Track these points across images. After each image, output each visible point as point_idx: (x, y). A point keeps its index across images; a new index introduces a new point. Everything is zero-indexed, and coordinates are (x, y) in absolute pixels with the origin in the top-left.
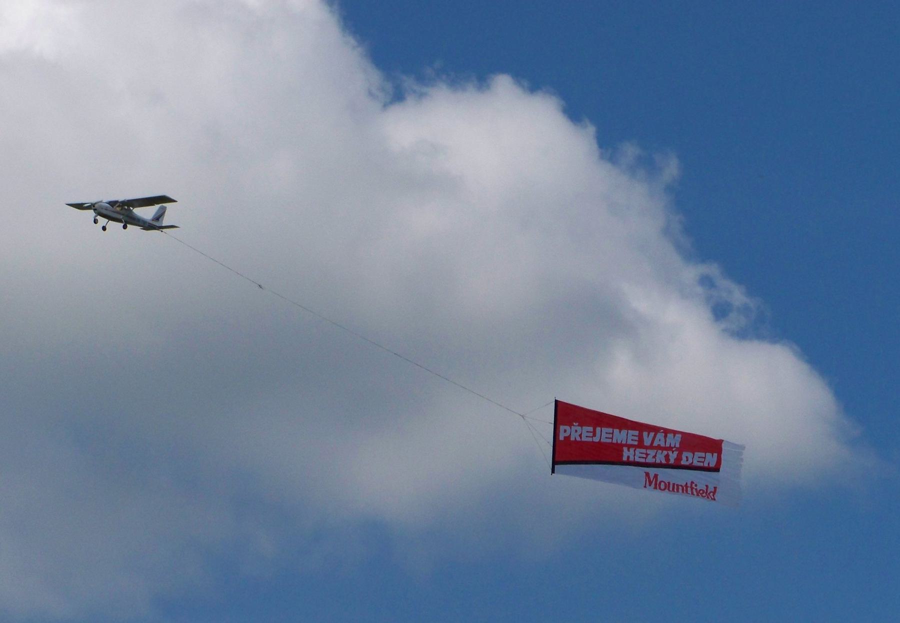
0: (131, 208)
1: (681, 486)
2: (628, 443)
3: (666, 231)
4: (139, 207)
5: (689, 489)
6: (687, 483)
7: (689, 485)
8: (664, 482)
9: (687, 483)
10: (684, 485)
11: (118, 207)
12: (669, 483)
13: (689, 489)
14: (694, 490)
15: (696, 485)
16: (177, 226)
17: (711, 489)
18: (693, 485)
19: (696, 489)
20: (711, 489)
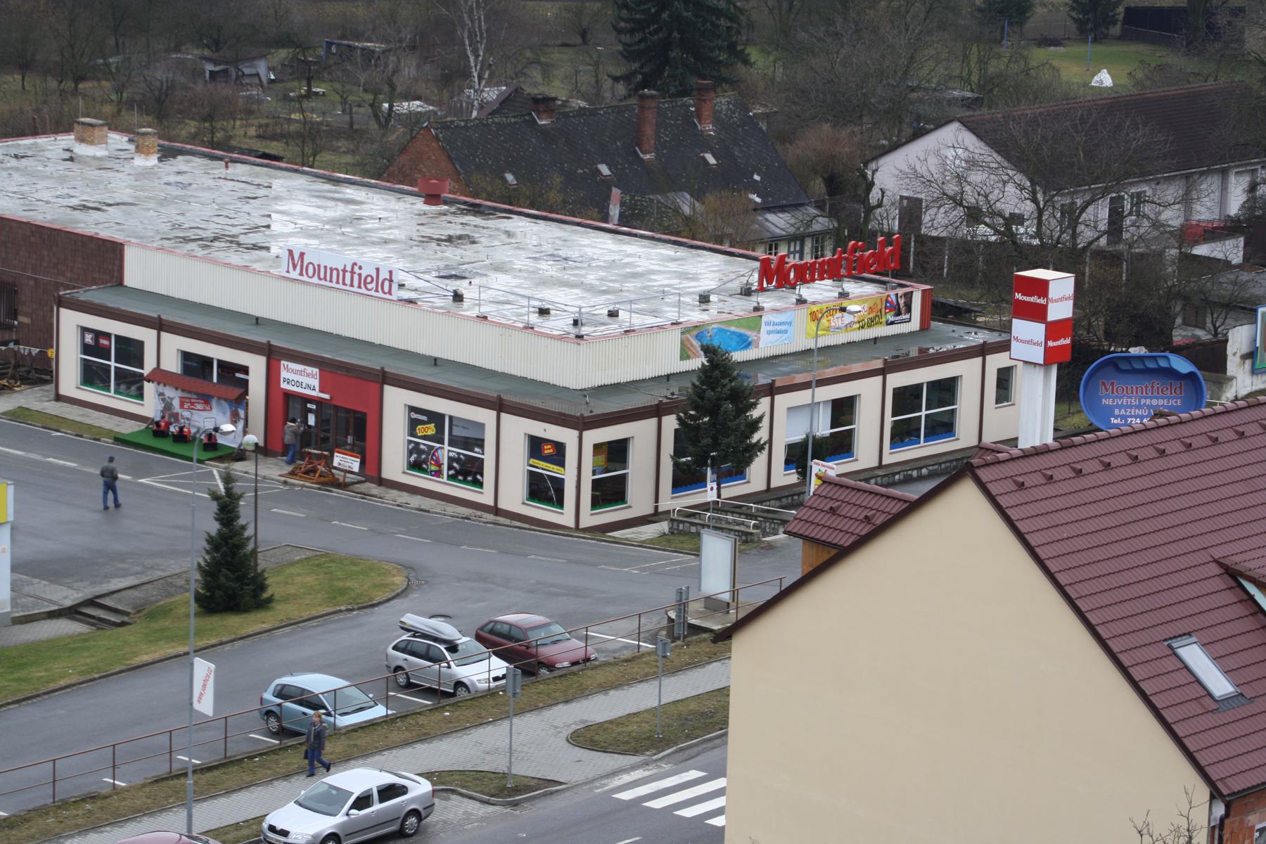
0: (208, 594)
1: (337, 269)
2: (885, 462)
3: (441, 740)
4: (998, 378)
5: (348, 275)
6: (345, 266)
7: (349, 268)
8: (313, 265)
9: (345, 266)
10: (340, 268)
11: (351, 808)
12: (319, 266)
13: (348, 275)
14: (356, 278)
15: (360, 268)
16: (561, 780)
17: (384, 275)
18: (356, 269)
19: (360, 275)
20: (384, 275)
